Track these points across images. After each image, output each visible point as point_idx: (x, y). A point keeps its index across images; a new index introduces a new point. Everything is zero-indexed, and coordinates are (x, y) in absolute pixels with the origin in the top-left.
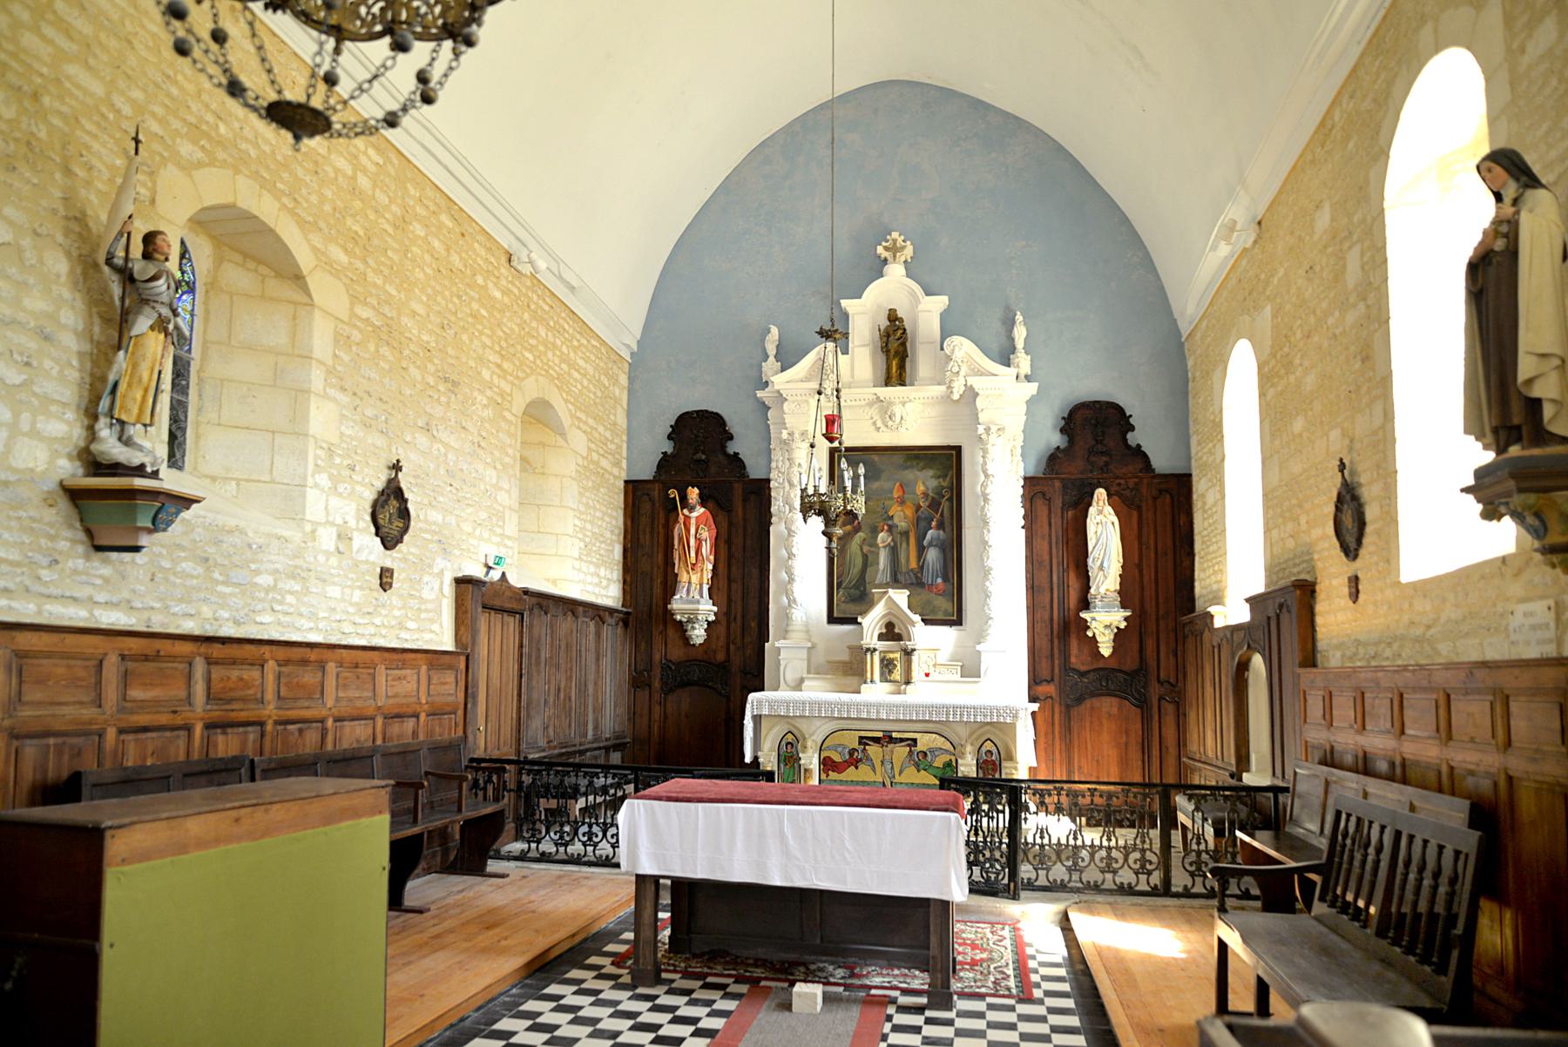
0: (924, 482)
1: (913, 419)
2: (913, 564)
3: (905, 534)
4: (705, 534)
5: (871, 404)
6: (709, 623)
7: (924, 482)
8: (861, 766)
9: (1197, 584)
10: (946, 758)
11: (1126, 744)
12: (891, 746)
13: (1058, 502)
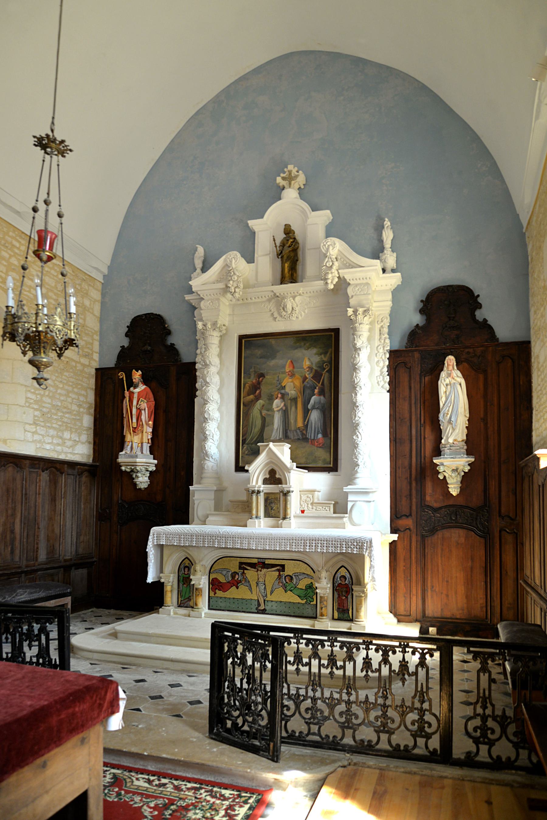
0: (309, 359)
1: (301, 310)
2: (300, 424)
3: (294, 400)
4: (144, 405)
5: (269, 300)
6: (151, 472)
7: (309, 359)
8: (241, 587)
9: (534, 434)
10: (307, 581)
11: (472, 568)
12: (264, 570)
13: (417, 370)
